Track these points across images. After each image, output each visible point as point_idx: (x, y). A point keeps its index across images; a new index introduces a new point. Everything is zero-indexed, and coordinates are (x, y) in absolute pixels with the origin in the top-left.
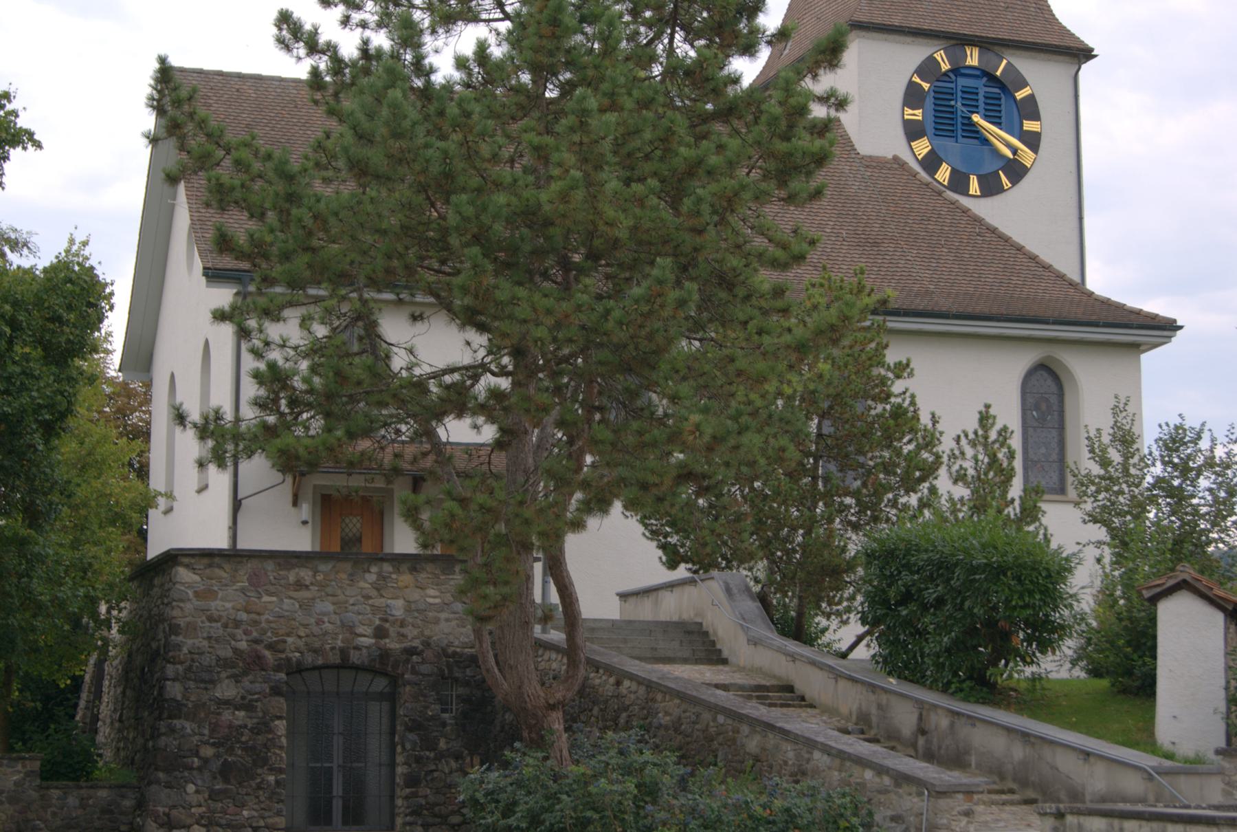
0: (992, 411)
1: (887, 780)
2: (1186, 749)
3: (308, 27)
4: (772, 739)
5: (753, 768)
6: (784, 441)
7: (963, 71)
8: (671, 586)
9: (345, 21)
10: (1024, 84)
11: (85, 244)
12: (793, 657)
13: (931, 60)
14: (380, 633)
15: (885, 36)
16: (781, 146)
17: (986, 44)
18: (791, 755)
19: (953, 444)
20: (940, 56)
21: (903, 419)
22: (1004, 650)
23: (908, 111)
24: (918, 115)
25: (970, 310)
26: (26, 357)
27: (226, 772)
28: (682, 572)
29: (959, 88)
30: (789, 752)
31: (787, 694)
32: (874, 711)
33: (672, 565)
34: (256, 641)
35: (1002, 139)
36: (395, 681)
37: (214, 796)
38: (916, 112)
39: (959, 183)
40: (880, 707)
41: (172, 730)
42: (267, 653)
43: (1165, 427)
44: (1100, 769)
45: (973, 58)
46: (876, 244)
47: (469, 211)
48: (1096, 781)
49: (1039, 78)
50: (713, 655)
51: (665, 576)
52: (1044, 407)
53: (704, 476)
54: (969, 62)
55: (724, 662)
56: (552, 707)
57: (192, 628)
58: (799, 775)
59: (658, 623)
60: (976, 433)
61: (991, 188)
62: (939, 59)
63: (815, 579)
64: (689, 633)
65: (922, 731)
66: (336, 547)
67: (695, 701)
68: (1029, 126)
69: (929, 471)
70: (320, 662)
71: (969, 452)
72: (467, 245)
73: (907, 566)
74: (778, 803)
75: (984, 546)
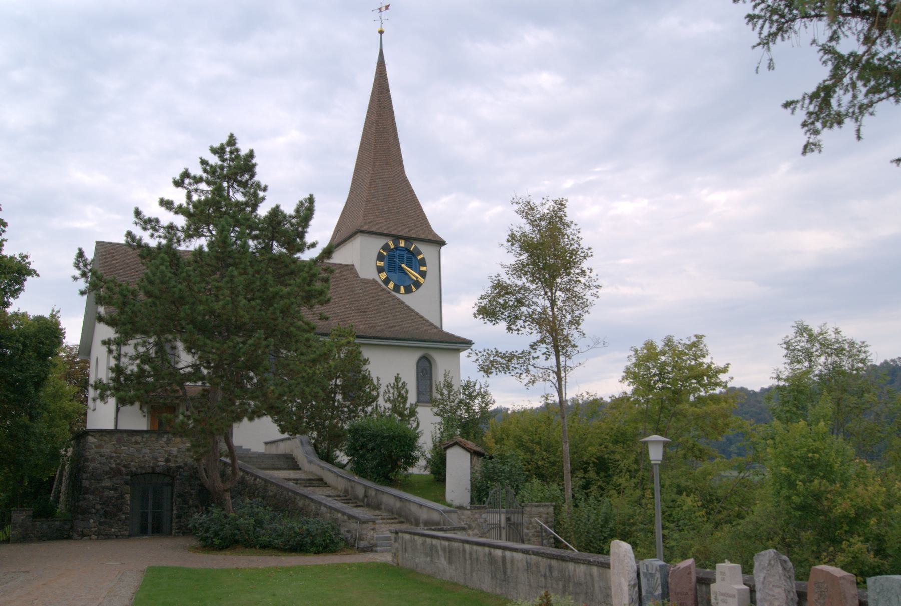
1: (346, 518)
2: (456, 503)
3: (138, 238)
4: (307, 502)
6: (319, 390)
8: (282, 440)
9: (152, 236)
10: (421, 254)
11: (58, 311)
12: (323, 468)
14: (167, 460)
16: (307, 288)
17: (408, 239)
20: (391, 243)
21: (367, 379)
22: (395, 466)
24: (382, 264)
26: (30, 357)
27: (106, 514)
28: (286, 435)
30: (313, 506)
31: (320, 482)
32: (350, 489)
33: (283, 432)
34: (118, 464)
35: (414, 275)
36: (173, 478)
37: (100, 524)
39: (397, 289)
41: (84, 499)
42: (123, 469)
44: (425, 510)
45: (402, 244)
46: (365, 312)
47: (189, 311)
48: (424, 515)
49: (426, 252)
50: (296, 467)
55: (300, 469)
56: (226, 491)
57: (93, 460)
58: (317, 515)
59: (276, 455)
61: (408, 291)
63: (335, 438)
65: (366, 496)
66: (156, 428)
67: (281, 487)
68: (423, 269)
69: (375, 399)
70: (144, 472)
71: (392, 391)
72: (188, 324)
73: (363, 436)
74: (305, 527)
75: (388, 429)
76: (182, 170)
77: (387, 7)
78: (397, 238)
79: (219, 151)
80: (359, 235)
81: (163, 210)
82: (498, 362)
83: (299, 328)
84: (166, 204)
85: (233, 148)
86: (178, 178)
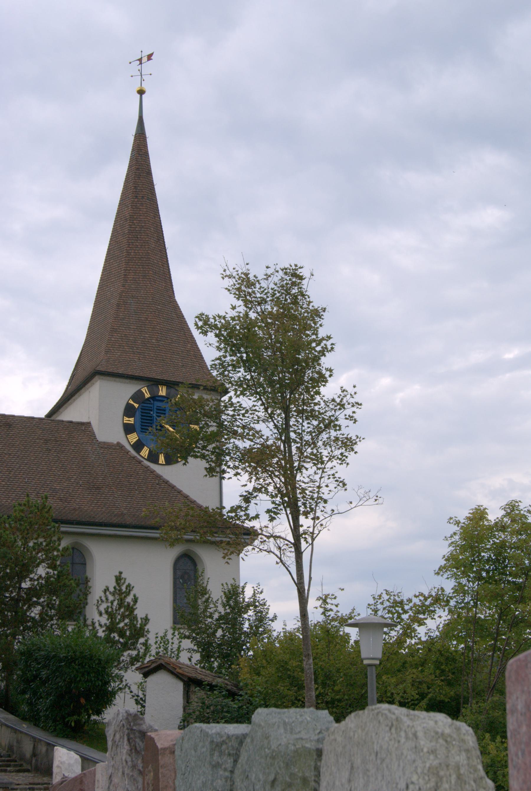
0: (123, 576)
7: (157, 398)
13: (139, 392)
15: (114, 379)
17: (170, 385)
19: (102, 594)
23: (126, 419)
24: (131, 420)
25: (143, 523)
29: (155, 407)
32: (15, 744)
38: (130, 419)
39: (153, 458)
40: (18, 742)
43: (225, 585)
45: (163, 391)
46: (98, 488)
52: (186, 577)
54: (161, 393)
60: (115, 588)
61: (169, 461)
62: (144, 391)
65: (34, 754)
71: (111, 598)
77: (150, 57)
78: (154, 383)
80: (97, 377)
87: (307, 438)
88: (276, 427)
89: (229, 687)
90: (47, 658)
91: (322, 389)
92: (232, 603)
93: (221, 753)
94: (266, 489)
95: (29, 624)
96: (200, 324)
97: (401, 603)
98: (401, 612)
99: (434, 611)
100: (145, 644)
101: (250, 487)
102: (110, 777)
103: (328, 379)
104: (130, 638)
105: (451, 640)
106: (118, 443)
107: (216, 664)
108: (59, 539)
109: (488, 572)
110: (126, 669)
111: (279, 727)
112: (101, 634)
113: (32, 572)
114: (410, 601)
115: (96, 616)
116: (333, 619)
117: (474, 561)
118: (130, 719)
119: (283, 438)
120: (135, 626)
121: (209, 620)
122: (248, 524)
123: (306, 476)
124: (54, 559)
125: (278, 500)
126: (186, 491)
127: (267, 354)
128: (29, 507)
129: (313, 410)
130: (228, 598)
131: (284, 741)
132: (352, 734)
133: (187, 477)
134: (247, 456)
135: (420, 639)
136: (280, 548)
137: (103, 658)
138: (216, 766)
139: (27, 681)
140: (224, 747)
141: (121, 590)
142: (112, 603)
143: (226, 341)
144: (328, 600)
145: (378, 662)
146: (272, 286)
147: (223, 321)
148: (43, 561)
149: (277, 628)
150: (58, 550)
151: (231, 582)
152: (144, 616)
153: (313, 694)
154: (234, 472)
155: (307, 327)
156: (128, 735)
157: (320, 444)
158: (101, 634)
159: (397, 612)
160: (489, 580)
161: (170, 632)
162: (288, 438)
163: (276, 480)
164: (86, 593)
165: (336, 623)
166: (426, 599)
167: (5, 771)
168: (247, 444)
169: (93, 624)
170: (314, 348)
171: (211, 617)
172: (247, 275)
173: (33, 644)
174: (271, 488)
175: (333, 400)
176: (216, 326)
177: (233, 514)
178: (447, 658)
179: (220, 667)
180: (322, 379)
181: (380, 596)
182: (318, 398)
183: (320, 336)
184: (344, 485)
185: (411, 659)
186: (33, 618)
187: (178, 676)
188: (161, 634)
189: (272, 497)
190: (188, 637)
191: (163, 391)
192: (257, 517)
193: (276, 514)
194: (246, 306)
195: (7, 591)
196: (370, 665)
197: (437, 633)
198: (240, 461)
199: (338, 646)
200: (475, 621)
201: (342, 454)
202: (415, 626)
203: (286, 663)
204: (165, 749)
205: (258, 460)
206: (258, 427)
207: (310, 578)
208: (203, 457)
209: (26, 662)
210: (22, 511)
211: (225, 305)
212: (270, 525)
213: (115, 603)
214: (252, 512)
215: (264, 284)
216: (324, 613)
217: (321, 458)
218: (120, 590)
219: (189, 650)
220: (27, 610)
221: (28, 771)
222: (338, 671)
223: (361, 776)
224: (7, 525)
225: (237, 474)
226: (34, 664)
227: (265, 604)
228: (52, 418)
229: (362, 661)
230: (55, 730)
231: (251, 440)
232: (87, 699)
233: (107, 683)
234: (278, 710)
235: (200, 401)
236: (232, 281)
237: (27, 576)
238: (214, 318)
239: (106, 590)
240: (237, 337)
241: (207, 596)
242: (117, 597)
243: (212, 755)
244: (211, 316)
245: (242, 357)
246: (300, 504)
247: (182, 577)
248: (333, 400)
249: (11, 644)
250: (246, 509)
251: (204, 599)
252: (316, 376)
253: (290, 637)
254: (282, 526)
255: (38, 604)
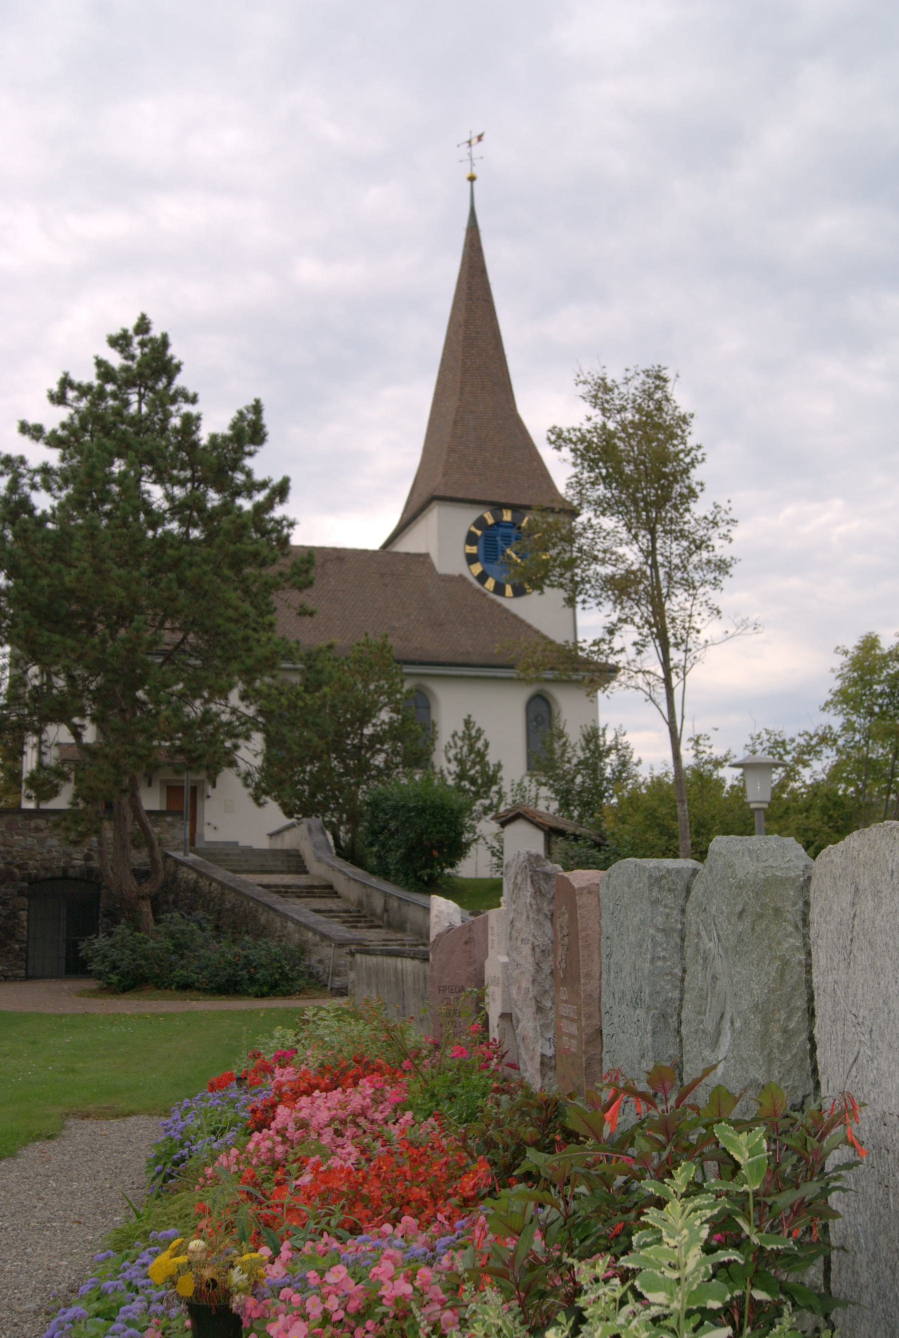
0: (472, 719)
1: (318, 938)
4: (272, 915)
5: (262, 932)
12: (333, 868)
17: (516, 509)
18: (279, 924)
19: (450, 740)
24: (473, 550)
32: (365, 899)
34: (10, 864)
39: (499, 589)
40: (368, 897)
42: (16, 871)
45: (507, 516)
51: (287, 821)
53: (190, 751)
61: (519, 592)
64: (289, 856)
65: (386, 910)
70: (49, 875)
71: (460, 743)
76: (59, 376)
77: (480, 138)
78: (497, 507)
79: (120, 342)
80: (434, 504)
81: (26, 439)
82: (56, 483)
83: (229, 619)
84: (33, 431)
85: (146, 337)
86: (56, 388)
87: (676, 561)
88: (641, 550)
89: (594, 837)
90: (395, 808)
91: (692, 506)
92: (592, 746)
93: (661, 888)
94: (632, 620)
95: (374, 773)
96: (553, 438)
97: (783, 743)
98: (782, 752)
99: (821, 752)
100: (499, 792)
101: (614, 618)
102: (512, 922)
103: (699, 494)
104: (482, 786)
105: (839, 782)
106: (461, 576)
107: (576, 813)
108: (402, 681)
109: (881, 706)
110: (479, 819)
111: (743, 854)
112: (450, 781)
113: (374, 716)
114: (793, 740)
115: (444, 763)
116: (706, 762)
117: (865, 694)
118: (533, 860)
119: (650, 562)
120: (487, 773)
121: (567, 766)
122: (612, 660)
123: (677, 603)
124: (397, 702)
125: (645, 631)
126: (536, 625)
127: (628, 469)
128: (369, 646)
129: (681, 530)
130: (588, 742)
131: (752, 869)
132: (855, 854)
133: (538, 610)
134: (610, 582)
135: (804, 782)
136: (649, 684)
137: (456, 807)
138: (655, 902)
139: (375, 833)
140: (663, 882)
141: (471, 735)
142: (461, 748)
143: (582, 456)
144: (701, 742)
145: (766, 806)
146: (632, 391)
147: (578, 434)
148: (385, 705)
149: (644, 774)
150: (401, 693)
151: (590, 724)
152: (496, 762)
153: (689, 842)
154: (596, 601)
155: (673, 436)
156: (532, 877)
157: (690, 567)
158: (450, 781)
159: (779, 753)
160: (883, 715)
161: (527, 779)
162: (655, 561)
163: (643, 608)
164: (432, 739)
165: (710, 767)
166: (811, 738)
167: (356, 927)
168: (606, 570)
169: (442, 771)
170: (682, 460)
171: (569, 762)
172: (603, 379)
173: (379, 793)
174: (637, 619)
175: (705, 518)
176: (571, 440)
177: (596, 648)
178: (835, 804)
179: (581, 816)
180: (692, 494)
181: (759, 736)
182: (687, 516)
183: (689, 445)
184: (719, 612)
185: (794, 804)
186: (377, 767)
187: (538, 826)
188: (517, 781)
189: (639, 628)
190: (545, 785)
191: (507, 516)
192: (622, 650)
193: (643, 646)
194: (604, 415)
195: (348, 738)
196: (759, 809)
197: (824, 776)
198: (602, 589)
199: (712, 792)
200: (867, 762)
201: (715, 578)
202: (800, 768)
203: (655, 810)
204: (582, 889)
205: (621, 587)
206: (621, 550)
207: (683, 717)
208: (561, 586)
209: (373, 813)
210: (361, 651)
211: (580, 416)
212: (638, 658)
213: (465, 749)
214: (617, 645)
215: (623, 389)
216: (696, 756)
217: (693, 582)
218: (470, 735)
219: (547, 798)
220: (370, 758)
221: (380, 927)
222: (713, 817)
223: (869, 897)
224: (346, 668)
225: (600, 603)
226: (381, 815)
227: (627, 748)
228: (388, 549)
229: (748, 804)
230: (406, 884)
231: (615, 566)
232: (441, 852)
233: (461, 834)
234: (739, 837)
235: (556, 524)
236: (587, 388)
237: (369, 721)
238: (569, 431)
239: (454, 735)
240: (597, 452)
241: (564, 740)
242: (467, 742)
243: (651, 890)
244: (564, 429)
245: (600, 473)
246: (670, 634)
247: (536, 719)
248: (705, 518)
249: (356, 794)
250: (610, 642)
251: (561, 743)
252: (685, 491)
253: (658, 784)
254: (651, 660)
255: (381, 750)
